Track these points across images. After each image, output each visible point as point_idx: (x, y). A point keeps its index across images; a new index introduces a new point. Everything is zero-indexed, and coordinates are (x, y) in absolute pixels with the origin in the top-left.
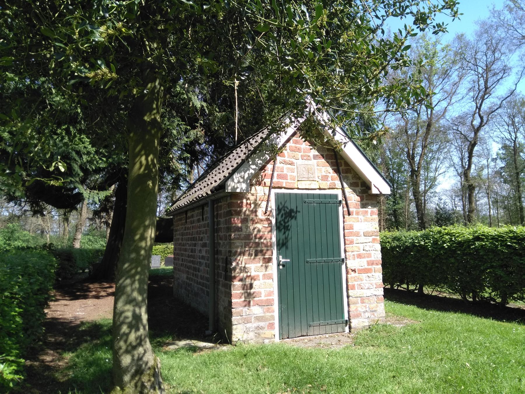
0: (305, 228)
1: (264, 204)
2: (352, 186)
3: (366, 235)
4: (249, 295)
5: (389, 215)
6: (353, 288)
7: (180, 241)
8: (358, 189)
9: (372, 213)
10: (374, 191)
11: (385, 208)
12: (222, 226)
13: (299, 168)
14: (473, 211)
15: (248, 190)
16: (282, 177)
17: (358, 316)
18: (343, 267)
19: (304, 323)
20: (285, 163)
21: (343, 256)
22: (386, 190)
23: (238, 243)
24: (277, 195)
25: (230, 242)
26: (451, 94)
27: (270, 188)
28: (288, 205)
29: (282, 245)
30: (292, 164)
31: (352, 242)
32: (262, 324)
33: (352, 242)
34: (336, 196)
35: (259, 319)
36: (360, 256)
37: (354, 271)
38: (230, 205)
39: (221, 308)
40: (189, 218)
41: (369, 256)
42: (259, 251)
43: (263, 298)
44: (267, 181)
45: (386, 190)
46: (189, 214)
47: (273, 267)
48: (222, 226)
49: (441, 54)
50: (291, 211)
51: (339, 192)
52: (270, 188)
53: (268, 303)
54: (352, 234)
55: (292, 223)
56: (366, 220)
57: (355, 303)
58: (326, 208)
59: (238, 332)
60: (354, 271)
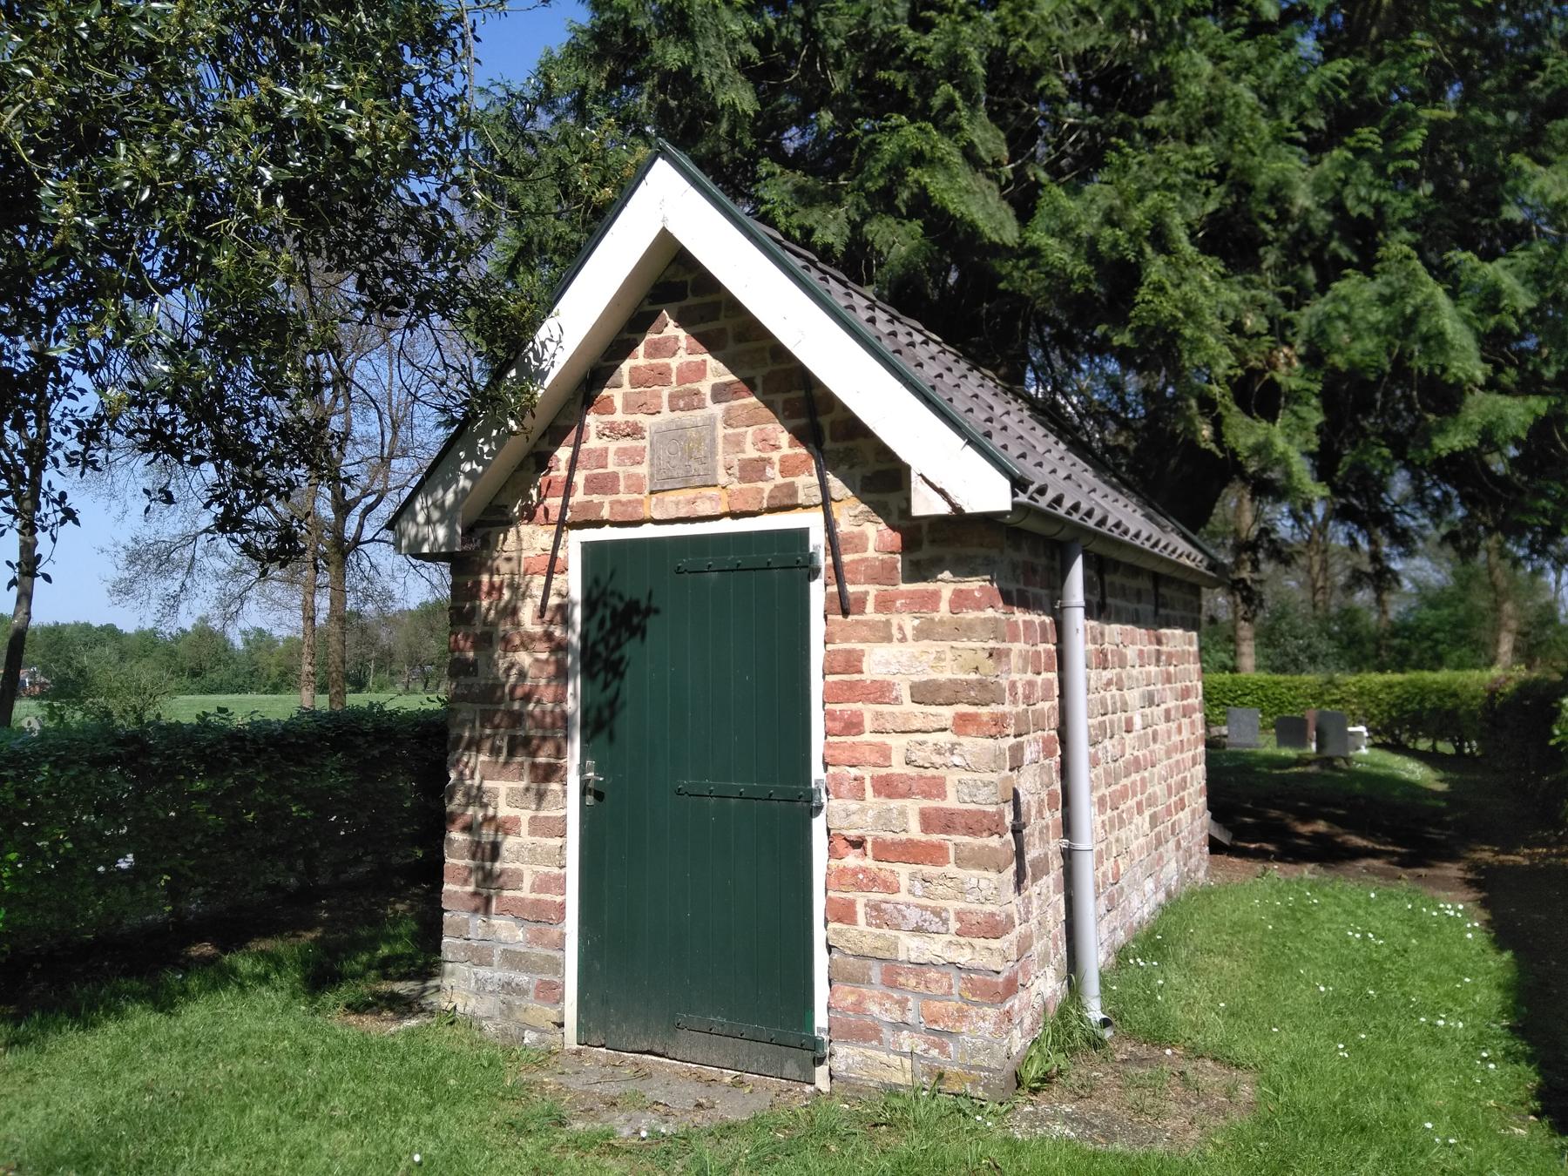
20: (613, 431)
27: (563, 525)
35: (514, 959)
37: (858, 844)
43: (526, 893)
47: (569, 802)
50: (633, 607)
51: (812, 521)
53: (542, 916)
55: (630, 649)
56: (923, 633)
58: (768, 575)
59: (461, 987)
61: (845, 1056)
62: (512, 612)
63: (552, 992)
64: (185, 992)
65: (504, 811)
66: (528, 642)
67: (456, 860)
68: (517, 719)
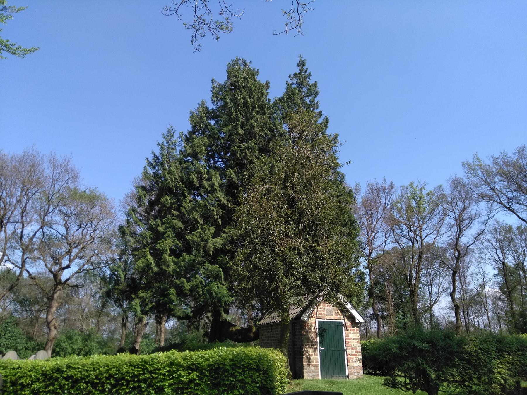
0: (330, 334)
1: (314, 325)
2: (348, 318)
3: (355, 339)
4: (309, 362)
5: (398, 328)
6: (350, 362)
7: (266, 341)
8: (351, 320)
9: (357, 330)
10: (357, 321)
11: (394, 321)
12: (297, 334)
13: (326, 312)
14: (459, 327)
15: (308, 320)
16: (320, 314)
17: (352, 374)
18: (345, 353)
19: (330, 375)
20: (321, 308)
21: (345, 348)
22: (362, 320)
23: (305, 341)
24: (319, 321)
25: (302, 341)
26: (437, 229)
27: (316, 319)
28: (323, 326)
29: (321, 343)
30: (324, 309)
31: (348, 342)
32: (315, 374)
33: (348, 342)
34: (342, 322)
35: (313, 372)
36: (352, 349)
37: (350, 355)
38: (302, 325)
39: (297, 368)
40: (274, 329)
41: (356, 349)
42: (313, 345)
43: (314, 363)
44: (315, 316)
45: (362, 320)
46: (274, 327)
47: (318, 352)
48: (297, 334)
49: (427, 198)
50: (324, 329)
51: (343, 321)
52: (316, 319)
53: (316, 366)
54: (348, 339)
55: (325, 334)
56: (354, 333)
57: (351, 369)
58: (338, 327)
59: (306, 376)
60: (350, 355)
61: (350, 377)
62: (310, 329)
63: (318, 375)
64: (380, 349)
65: (311, 353)
66: (313, 332)
67: (305, 360)
68: (312, 342)
